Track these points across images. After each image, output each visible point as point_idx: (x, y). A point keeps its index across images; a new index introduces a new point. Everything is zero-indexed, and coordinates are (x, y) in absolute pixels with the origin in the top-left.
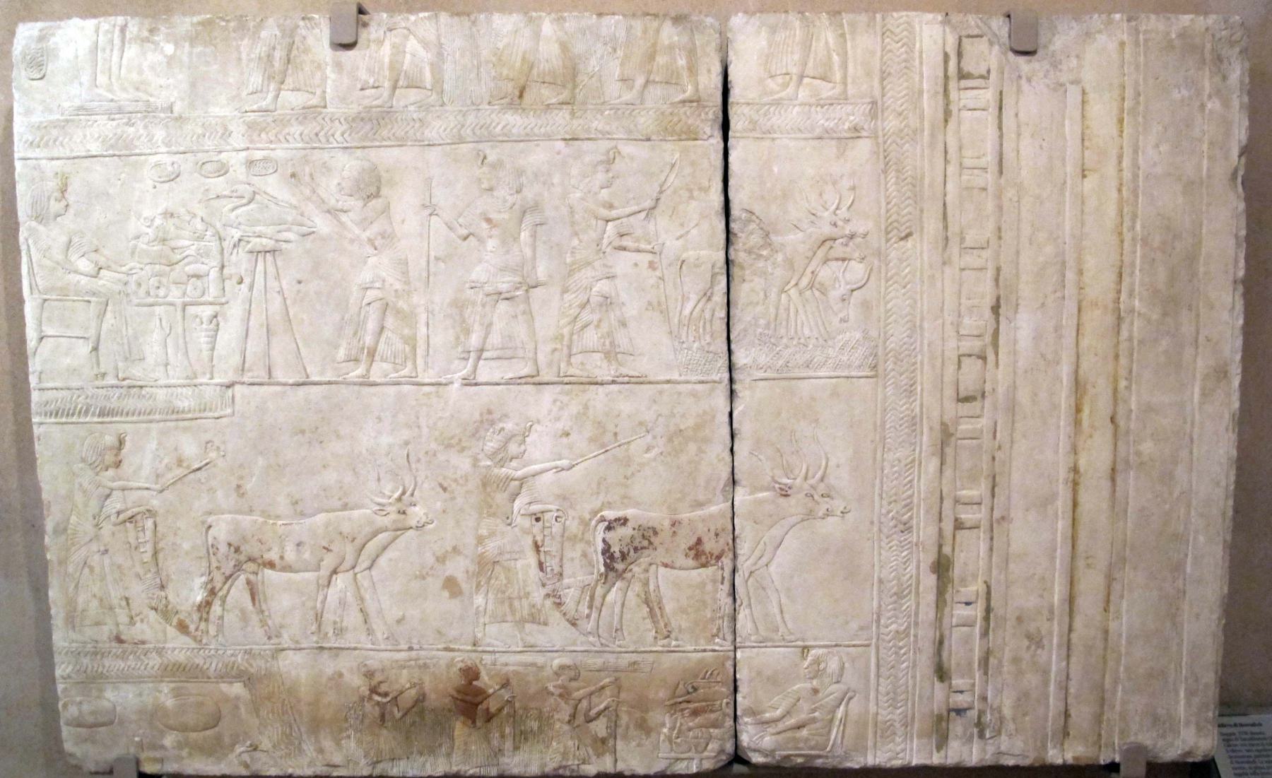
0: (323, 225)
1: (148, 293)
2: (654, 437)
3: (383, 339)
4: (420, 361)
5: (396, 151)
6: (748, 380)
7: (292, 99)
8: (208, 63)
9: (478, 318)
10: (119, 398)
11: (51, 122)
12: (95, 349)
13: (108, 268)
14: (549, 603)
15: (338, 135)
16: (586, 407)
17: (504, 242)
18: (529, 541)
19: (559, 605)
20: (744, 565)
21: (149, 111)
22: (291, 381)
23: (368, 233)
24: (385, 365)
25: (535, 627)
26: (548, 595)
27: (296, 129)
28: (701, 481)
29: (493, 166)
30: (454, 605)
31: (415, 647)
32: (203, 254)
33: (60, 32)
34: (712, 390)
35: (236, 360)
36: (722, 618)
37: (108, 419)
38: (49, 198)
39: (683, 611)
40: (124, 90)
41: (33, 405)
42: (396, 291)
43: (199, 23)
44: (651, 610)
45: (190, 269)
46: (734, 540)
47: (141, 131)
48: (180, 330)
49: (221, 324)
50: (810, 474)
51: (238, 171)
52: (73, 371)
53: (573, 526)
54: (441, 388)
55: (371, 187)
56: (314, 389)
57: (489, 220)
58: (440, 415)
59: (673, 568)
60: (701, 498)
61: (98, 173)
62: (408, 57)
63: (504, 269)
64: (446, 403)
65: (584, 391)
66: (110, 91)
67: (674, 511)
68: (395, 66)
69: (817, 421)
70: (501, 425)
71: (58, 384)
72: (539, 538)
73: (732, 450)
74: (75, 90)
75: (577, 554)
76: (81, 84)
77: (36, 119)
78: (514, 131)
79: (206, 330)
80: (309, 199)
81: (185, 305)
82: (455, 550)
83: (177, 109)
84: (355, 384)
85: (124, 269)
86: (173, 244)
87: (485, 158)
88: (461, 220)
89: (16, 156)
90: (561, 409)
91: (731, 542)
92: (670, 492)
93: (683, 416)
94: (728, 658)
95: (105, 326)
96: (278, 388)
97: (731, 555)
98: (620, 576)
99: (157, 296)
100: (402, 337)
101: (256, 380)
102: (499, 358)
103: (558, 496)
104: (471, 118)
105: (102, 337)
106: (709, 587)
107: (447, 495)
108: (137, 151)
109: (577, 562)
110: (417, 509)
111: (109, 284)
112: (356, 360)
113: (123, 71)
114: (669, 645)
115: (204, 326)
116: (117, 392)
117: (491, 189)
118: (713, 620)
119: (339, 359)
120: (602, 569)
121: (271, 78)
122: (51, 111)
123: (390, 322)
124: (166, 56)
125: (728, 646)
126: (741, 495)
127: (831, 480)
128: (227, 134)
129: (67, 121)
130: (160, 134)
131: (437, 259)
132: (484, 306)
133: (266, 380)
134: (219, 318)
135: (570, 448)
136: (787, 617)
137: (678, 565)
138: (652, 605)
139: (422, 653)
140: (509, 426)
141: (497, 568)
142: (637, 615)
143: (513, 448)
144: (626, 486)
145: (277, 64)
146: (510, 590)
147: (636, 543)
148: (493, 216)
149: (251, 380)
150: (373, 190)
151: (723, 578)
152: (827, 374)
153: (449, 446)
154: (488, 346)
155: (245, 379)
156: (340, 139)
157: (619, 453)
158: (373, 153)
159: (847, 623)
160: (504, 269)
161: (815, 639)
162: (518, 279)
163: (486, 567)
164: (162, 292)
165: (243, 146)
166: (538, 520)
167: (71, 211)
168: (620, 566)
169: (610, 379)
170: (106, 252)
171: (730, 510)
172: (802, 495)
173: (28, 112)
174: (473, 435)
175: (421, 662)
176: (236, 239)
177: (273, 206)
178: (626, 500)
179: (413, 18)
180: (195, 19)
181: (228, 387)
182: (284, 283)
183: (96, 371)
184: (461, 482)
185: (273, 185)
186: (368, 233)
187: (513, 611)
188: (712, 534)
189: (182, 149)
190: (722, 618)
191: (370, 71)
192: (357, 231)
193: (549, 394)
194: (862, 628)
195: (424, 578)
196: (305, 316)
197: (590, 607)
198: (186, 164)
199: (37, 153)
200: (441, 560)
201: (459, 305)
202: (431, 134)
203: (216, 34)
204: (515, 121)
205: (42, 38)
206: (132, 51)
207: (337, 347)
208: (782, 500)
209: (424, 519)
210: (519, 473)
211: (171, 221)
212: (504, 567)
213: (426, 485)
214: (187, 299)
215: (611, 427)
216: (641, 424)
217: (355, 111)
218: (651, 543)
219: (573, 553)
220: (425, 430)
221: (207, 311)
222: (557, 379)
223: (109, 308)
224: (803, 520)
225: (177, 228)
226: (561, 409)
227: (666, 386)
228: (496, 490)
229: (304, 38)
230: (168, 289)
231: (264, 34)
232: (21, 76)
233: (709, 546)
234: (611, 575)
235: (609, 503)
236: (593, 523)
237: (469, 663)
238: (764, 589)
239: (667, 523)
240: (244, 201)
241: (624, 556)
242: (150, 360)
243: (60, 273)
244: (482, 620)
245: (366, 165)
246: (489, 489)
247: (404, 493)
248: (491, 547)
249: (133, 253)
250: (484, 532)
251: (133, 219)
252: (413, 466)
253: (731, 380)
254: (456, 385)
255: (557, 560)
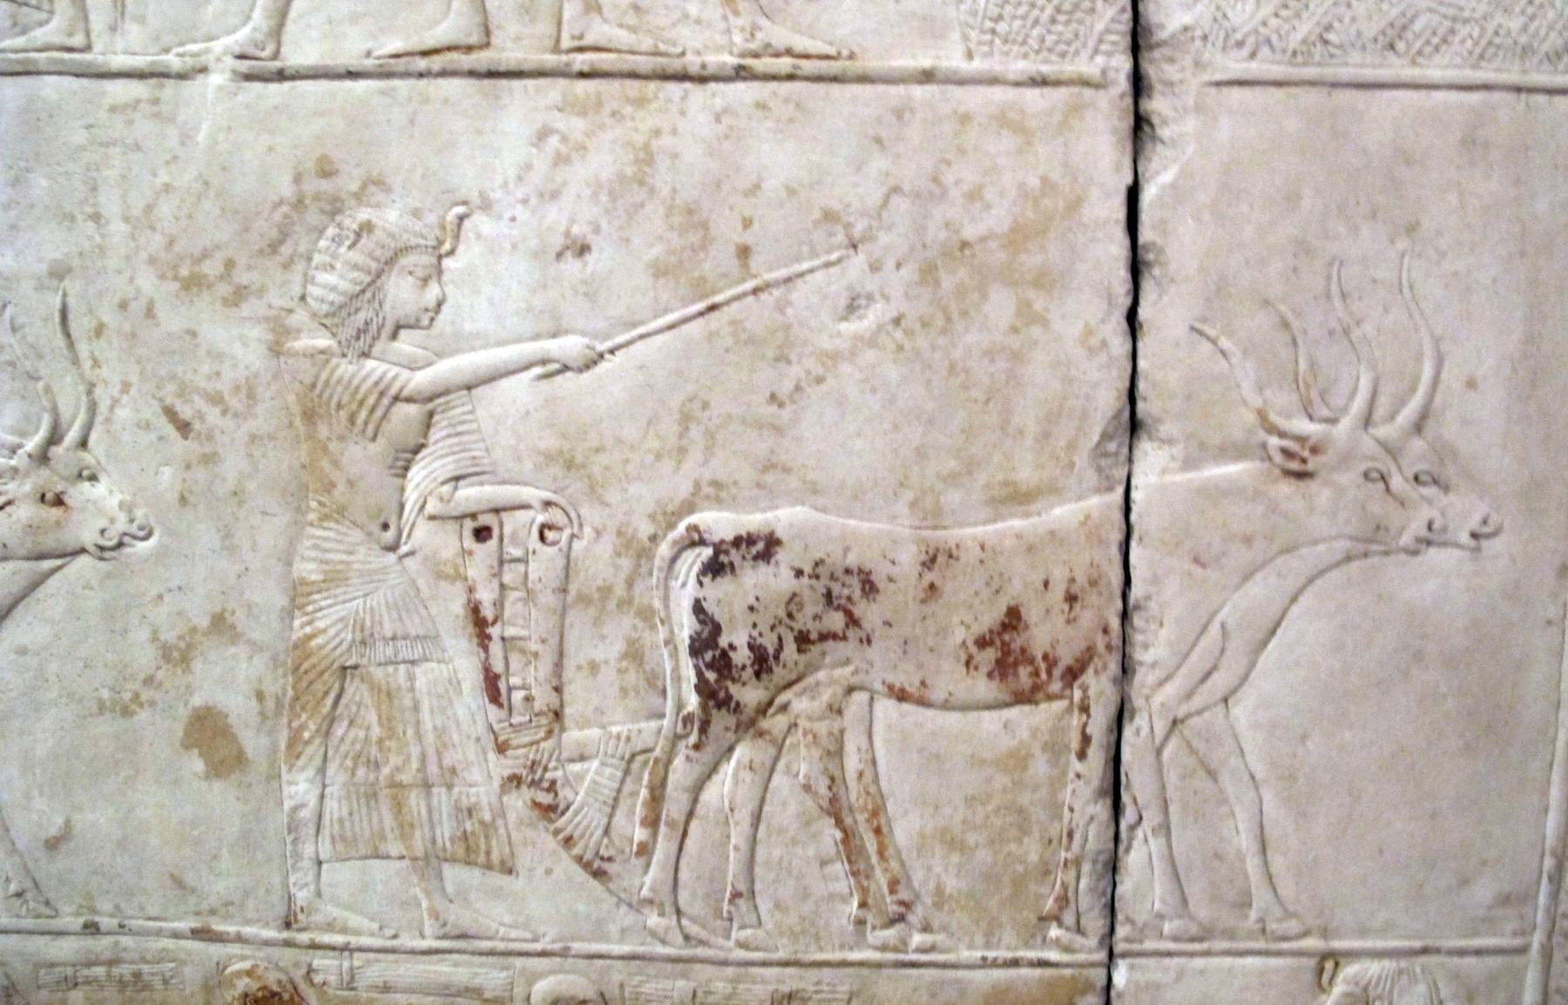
2: (875, 267)
6: (1194, 82)
14: (518, 803)
16: (646, 158)
18: (458, 606)
19: (549, 811)
20: (1155, 698)
25: (473, 876)
26: (515, 780)
28: (1028, 417)
30: (221, 801)
31: (106, 922)
34: (1076, 109)
36: (1078, 863)
39: (953, 843)
44: (848, 836)
46: (1125, 616)
50: (1380, 412)
53: (598, 559)
54: (170, 88)
58: (163, 177)
59: (923, 702)
60: (1026, 474)
64: (186, 138)
65: (641, 102)
67: (934, 516)
69: (1412, 229)
70: (364, 214)
72: (486, 596)
73: (1132, 317)
75: (611, 650)
82: (220, 624)
90: (560, 160)
91: (1115, 623)
92: (921, 453)
93: (974, 195)
94: (1088, 987)
97: (1114, 667)
98: (749, 725)
103: (549, 457)
106: (1040, 767)
107: (192, 447)
109: (608, 675)
110: (100, 490)
114: (902, 946)
118: (1046, 871)
120: (693, 702)
125: (1089, 949)
126: (1153, 468)
127: (1448, 428)
135: (590, 292)
136: (1278, 862)
137: (938, 695)
138: (854, 824)
139: (126, 941)
140: (390, 217)
141: (353, 688)
142: (801, 853)
143: (401, 293)
144: (778, 430)
146: (395, 760)
147: (804, 621)
151: (1086, 739)
152: (1452, 75)
153: (193, 284)
157: (757, 314)
159: (1464, 882)
161: (1363, 932)
163: (317, 686)
166: (482, 534)
168: (749, 694)
169: (731, 61)
171: (1118, 516)
172: (1348, 478)
174: (274, 247)
175: (125, 970)
178: (772, 475)
184: (235, 403)
187: (405, 829)
188: (1058, 593)
190: (1078, 863)
193: (523, 106)
194: (1505, 900)
195: (126, 712)
197: (652, 822)
200: (179, 655)
208: (1286, 488)
209: (121, 525)
210: (421, 380)
212: (375, 688)
213: (122, 413)
215: (728, 231)
216: (829, 216)
218: (853, 621)
219: (598, 644)
220: (118, 228)
222: (551, 60)
224: (1349, 558)
226: (560, 160)
227: (918, 91)
228: (352, 431)
233: (1047, 632)
234: (722, 721)
235: (717, 484)
236: (664, 550)
237: (272, 979)
238: (1212, 774)
239: (908, 557)
241: (762, 662)
244: (308, 850)
246: (323, 431)
247: (54, 438)
248: (329, 622)
250: (307, 569)
252: (83, 349)
253: (1138, 84)
255: (544, 668)
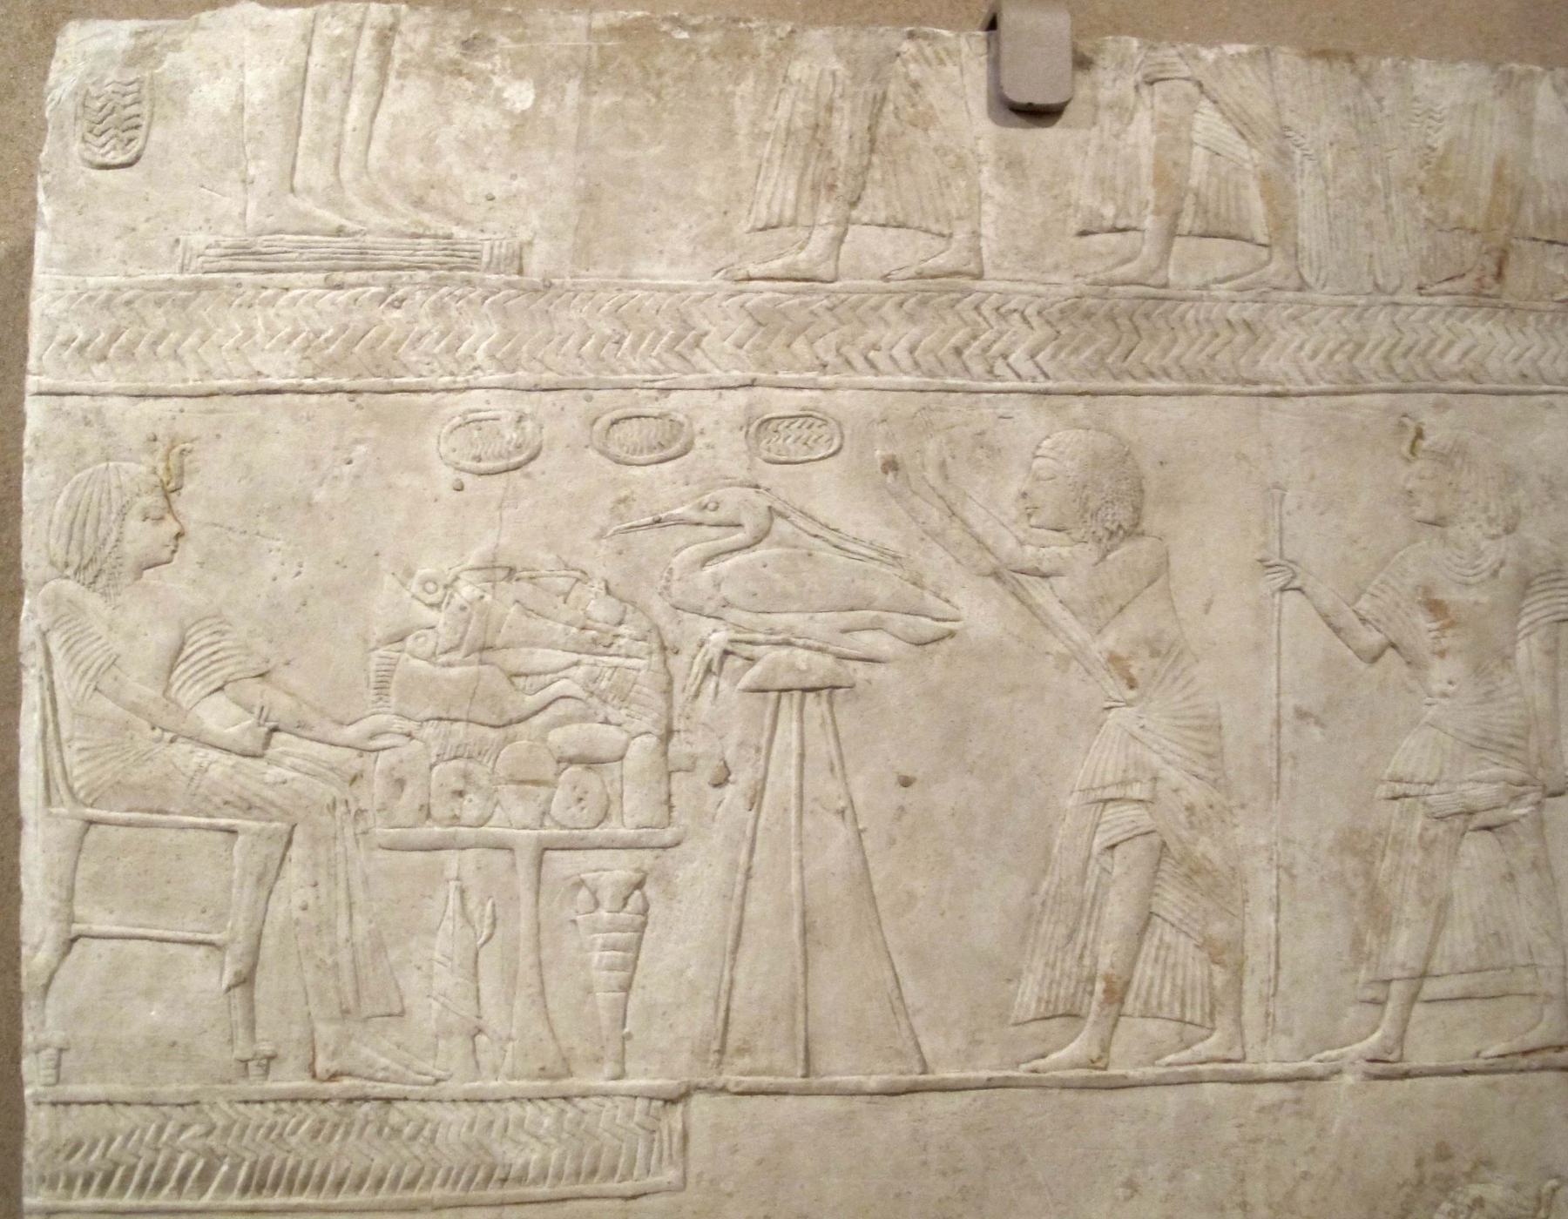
0: (979, 612)
1: (426, 812)
3: (1149, 949)
4: (1252, 1013)
5: (1180, 409)
7: (879, 250)
8: (633, 139)
9: (1413, 883)
10: (315, 1133)
11: (147, 288)
12: (246, 980)
13: (300, 728)
15: (1018, 357)
17: (1478, 670)
21: (454, 264)
22: (873, 1083)
23: (1110, 640)
24: (1152, 1026)
27: (897, 336)
29: (1444, 458)
32: (599, 699)
33: (197, 37)
35: (698, 1019)
37: (278, 1200)
38: (123, 514)
40: (377, 202)
41: (29, 1154)
42: (1190, 809)
43: (613, 30)
45: (564, 738)
47: (426, 324)
48: (524, 927)
49: (654, 910)
51: (721, 449)
52: (170, 1048)
55: (1120, 507)
56: (936, 1102)
57: (1435, 608)
61: (281, 437)
62: (1199, 154)
63: (1484, 743)
64: (1322, 1132)
66: (331, 204)
68: (1168, 178)
70: (1475, 1190)
71: (118, 1088)
74: (227, 202)
76: (247, 182)
77: (100, 279)
78: (1493, 364)
79: (614, 927)
80: (936, 536)
81: (544, 848)
83: (536, 264)
84: (1065, 1085)
85: (351, 733)
86: (513, 660)
87: (1420, 435)
88: (1364, 605)
89: (32, 383)
95: (279, 910)
96: (830, 1104)
99: (455, 819)
100: (1206, 944)
101: (766, 1081)
102: (1467, 997)
104: (1381, 322)
105: (269, 943)
108: (410, 380)
111: (300, 782)
112: (1074, 1016)
113: (377, 149)
115: (604, 914)
116: (310, 1116)
117: (1438, 522)
119: (1017, 1013)
121: (824, 187)
122: (147, 257)
123: (1171, 899)
124: (509, 114)
128: (687, 340)
129: (198, 286)
130: (482, 334)
131: (1301, 714)
132: (1427, 846)
133: (797, 1081)
134: (650, 890)
145: (841, 153)
148: (1450, 595)
149: (749, 1081)
150: (1123, 514)
154: (1438, 965)
155: (730, 1078)
156: (1026, 367)
158: (1120, 412)
160: (1484, 743)
162: (1515, 772)
164: (471, 807)
165: (737, 375)
167: (189, 551)
170: (292, 678)
173: (77, 261)
176: (714, 651)
177: (825, 553)
179: (1209, 55)
180: (599, 21)
181: (670, 1101)
182: (858, 781)
183: (242, 1049)
185: (830, 494)
186: (1110, 640)
189: (549, 377)
191: (1101, 183)
192: (1079, 633)
196: (919, 886)
198: (562, 419)
199: (99, 376)
201: (1359, 845)
202: (1273, 364)
203: (660, 61)
204: (1492, 342)
205: (140, 55)
206: (408, 99)
207: (1015, 976)
211: (510, 591)
214: (551, 832)
217: (1068, 290)
221: (617, 869)
223: (295, 852)
225: (527, 611)
229: (916, 85)
230: (491, 797)
231: (798, 70)
232: (64, 156)
240: (740, 537)
242: (426, 1014)
243: (144, 736)
245: (1104, 443)
249: (382, 687)
251: (389, 581)
254: (1348, 1079)
